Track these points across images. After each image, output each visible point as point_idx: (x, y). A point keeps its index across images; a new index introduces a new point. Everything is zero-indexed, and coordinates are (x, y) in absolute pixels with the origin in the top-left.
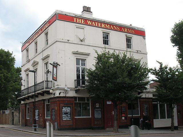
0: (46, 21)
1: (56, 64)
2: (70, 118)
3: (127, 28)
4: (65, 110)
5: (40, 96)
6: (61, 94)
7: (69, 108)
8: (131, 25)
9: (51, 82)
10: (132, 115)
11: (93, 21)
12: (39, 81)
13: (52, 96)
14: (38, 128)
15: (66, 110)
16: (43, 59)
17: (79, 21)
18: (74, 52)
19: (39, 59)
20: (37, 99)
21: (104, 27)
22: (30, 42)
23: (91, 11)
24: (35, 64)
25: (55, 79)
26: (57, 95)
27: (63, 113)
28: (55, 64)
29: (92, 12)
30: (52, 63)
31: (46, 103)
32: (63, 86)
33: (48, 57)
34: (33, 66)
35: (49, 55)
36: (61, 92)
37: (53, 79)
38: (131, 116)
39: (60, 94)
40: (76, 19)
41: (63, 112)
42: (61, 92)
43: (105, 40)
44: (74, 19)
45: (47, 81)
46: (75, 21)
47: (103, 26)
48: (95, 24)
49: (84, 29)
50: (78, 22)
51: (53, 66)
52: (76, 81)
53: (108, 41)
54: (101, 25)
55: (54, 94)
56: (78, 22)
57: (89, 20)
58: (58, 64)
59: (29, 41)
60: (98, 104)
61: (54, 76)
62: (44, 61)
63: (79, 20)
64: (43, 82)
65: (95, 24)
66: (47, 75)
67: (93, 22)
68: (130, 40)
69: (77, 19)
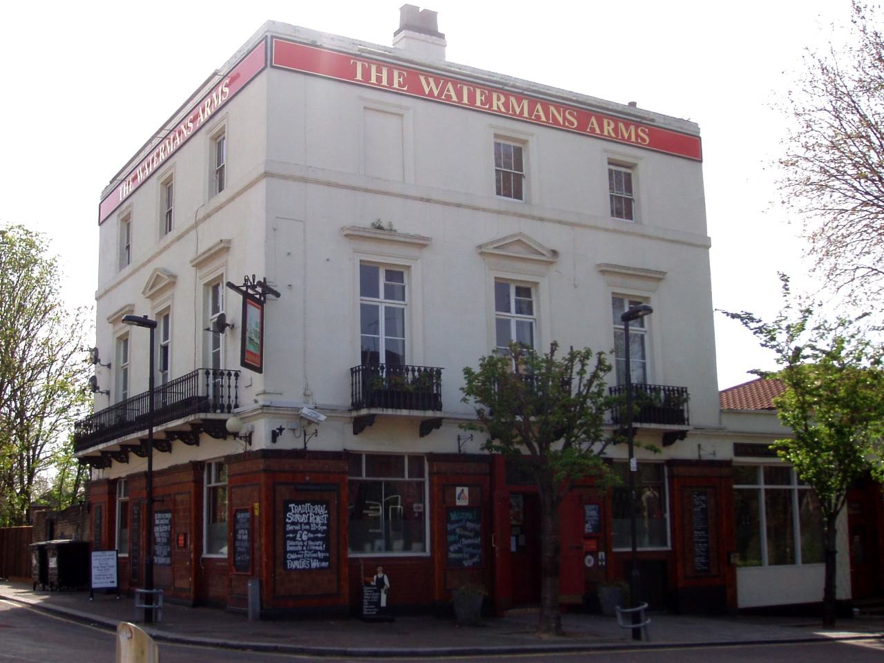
0: (215, 74)
1: (259, 289)
2: (325, 559)
3: (616, 120)
4: (297, 516)
5: (178, 445)
6: (279, 438)
7: (321, 509)
8: (633, 104)
9: (233, 378)
10: (634, 547)
11: (447, 79)
12: (178, 369)
13: (237, 447)
14: (160, 604)
15: (303, 519)
16: (199, 264)
17: (379, 79)
18: (607, 265)
19: (179, 259)
20: (161, 461)
21: (503, 110)
22: (141, 178)
23: (440, 31)
24: (162, 284)
25: (253, 361)
26: (261, 441)
27: (291, 532)
28: (253, 287)
29: (442, 36)
30: (239, 282)
31: (209, 482)
32: (292, 397)
33: (223, 248)
34: (152, 297)
35: (229, 241)
36: (281, 430)
37: (244, 364)
38: (629, 549)
39: (275, 436)
40: (469, 89)
41: (289, 528)
42: (281, 430)
43: (507, 175)
44: (355, 64)
45: (218, 373)
46: (359, 77)
47: (498, 103)
48: (460, 96)
49: (401, 116)
50: (373, 80)
51: (246, 296)
52: (359, 377)
53: (629, 202)
54: (489, 100)
55: (246, 437)
56: (373, 80)
57: (427, 75)
58: (267, 289)
59: (132, 175)
60: (466, 490)
61: (250, 347)
62: (206, 270)
63: (379, 71)
64: (194, 375)
65: (460, 96)
66: (216, 344)
67: (450, 86)
68: (628, 176)
69: (370, 67)
